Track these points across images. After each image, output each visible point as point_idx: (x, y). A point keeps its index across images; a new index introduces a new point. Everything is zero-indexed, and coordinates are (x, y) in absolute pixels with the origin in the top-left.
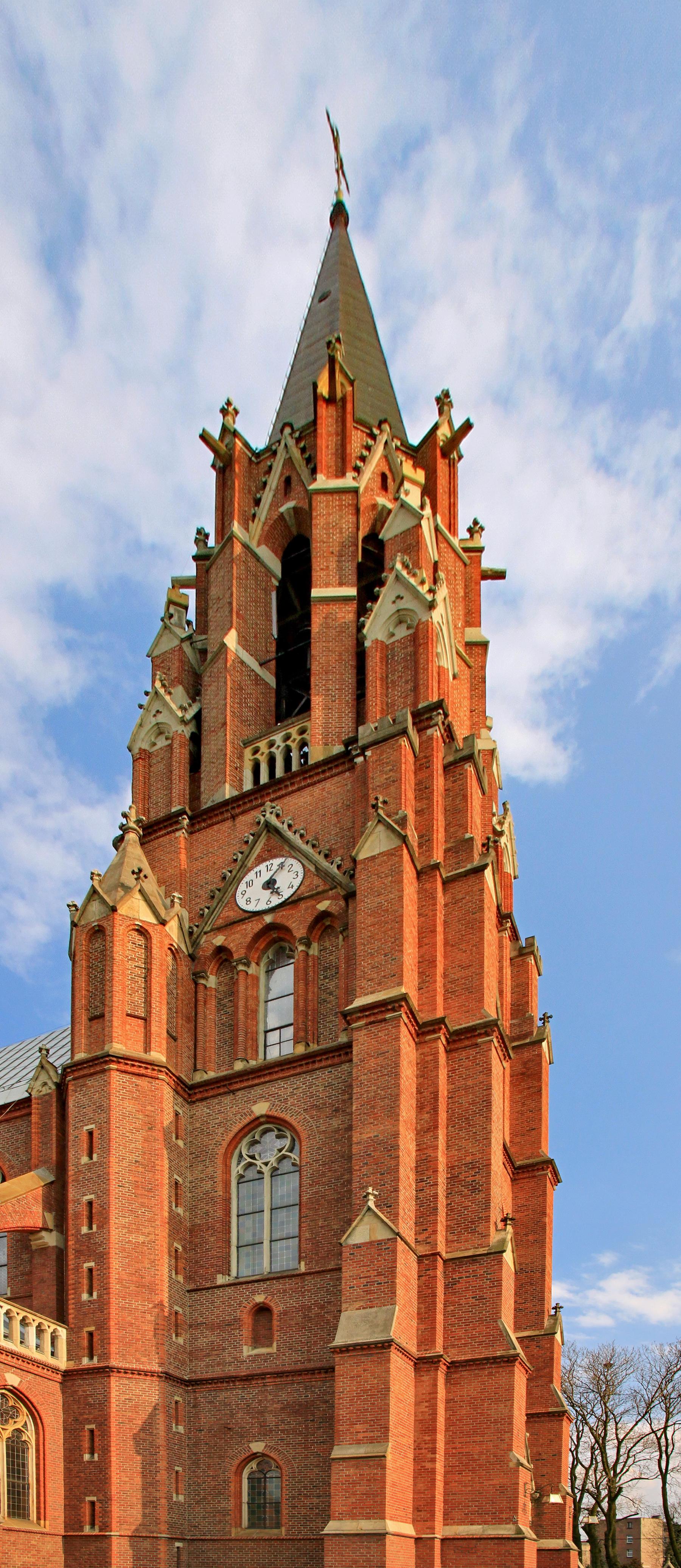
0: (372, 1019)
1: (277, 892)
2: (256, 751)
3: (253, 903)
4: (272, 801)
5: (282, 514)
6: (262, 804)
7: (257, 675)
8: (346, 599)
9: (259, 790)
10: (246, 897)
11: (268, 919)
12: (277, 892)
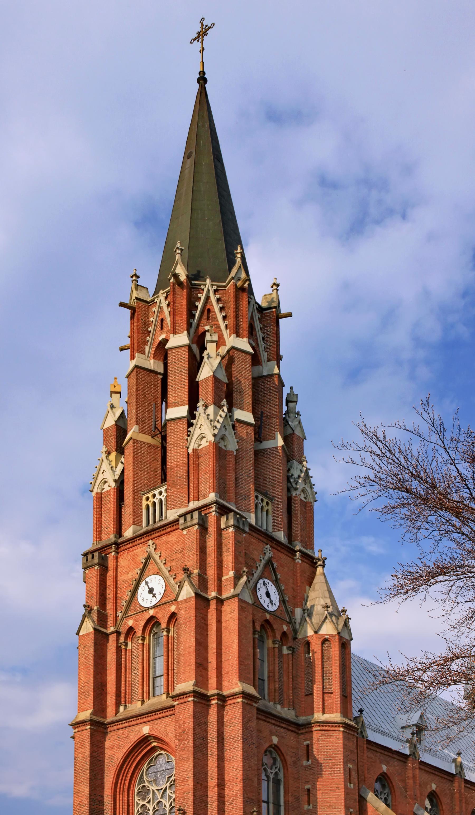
0: (181, 701)
1: (154, 596)
2: (148, 499)
3: (145, 601)
4: (152, 539)
5: (160, 341)
6: (148, 540)
7: (150, 446)
8: (183, 418)
9: (147, 533)
10: (142, 596)
11: (151, 612)
12: (154, 596)
